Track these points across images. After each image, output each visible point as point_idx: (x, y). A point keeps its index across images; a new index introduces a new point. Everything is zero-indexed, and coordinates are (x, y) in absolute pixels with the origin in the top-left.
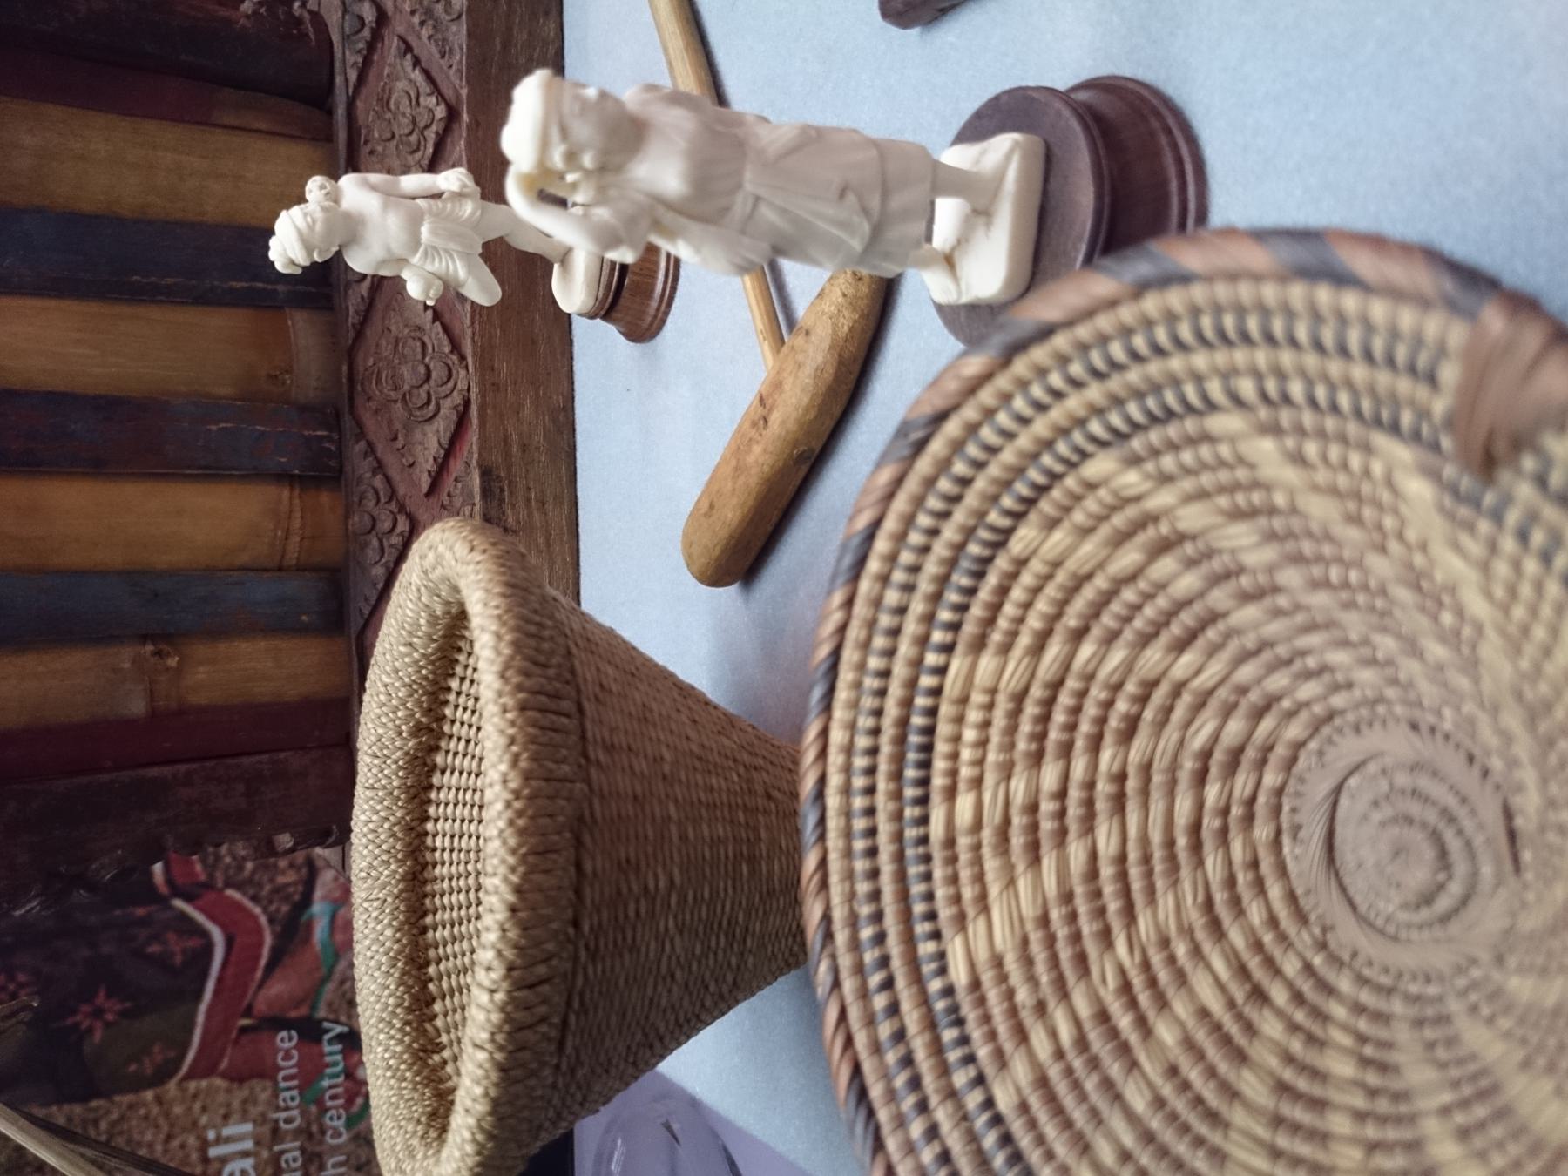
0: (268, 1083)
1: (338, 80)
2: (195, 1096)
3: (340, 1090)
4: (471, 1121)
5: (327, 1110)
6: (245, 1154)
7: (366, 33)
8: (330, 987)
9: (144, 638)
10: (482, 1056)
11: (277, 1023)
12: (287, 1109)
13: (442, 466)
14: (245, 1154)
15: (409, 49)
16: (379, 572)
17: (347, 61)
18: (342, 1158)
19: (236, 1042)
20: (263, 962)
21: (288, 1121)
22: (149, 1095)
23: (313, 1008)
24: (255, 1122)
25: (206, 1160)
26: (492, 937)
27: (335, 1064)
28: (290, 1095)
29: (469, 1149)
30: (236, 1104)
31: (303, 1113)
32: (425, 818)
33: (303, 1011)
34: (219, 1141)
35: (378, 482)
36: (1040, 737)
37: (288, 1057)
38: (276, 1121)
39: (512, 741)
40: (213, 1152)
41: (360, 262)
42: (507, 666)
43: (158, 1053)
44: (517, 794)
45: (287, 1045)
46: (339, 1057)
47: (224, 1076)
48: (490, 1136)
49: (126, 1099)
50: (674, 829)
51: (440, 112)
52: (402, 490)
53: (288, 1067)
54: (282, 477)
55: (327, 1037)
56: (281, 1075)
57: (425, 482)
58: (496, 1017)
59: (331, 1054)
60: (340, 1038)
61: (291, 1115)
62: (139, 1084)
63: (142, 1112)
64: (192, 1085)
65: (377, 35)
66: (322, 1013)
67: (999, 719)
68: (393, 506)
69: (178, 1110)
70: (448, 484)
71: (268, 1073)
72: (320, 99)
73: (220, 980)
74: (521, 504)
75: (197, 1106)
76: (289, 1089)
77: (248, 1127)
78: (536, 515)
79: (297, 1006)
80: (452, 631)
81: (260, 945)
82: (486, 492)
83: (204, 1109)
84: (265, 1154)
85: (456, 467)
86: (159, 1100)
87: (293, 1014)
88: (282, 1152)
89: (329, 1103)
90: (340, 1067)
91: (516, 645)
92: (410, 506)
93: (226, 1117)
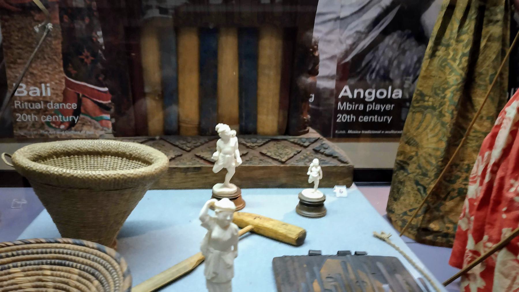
0: (62, 101)
1: (291, 137)
2: (60, 81)
3: (58, 120)
4: (32, 166)
5: (52, 116)
6: (41, 93)
7: (302, 143)
8: (89, 118)
9: (162, 92)
10: (45, 169)
11: (79, 102)
12: (54, 106)
13: (202, 158)
14: (41, 93)
15: (299, 153)
16: (177, 143)
17: (296, 139)
18: (37, 120)
19: (76, 93)
20: (98, 101)
21: (50, 106)
22: (62, 69)
23: (83, 114)
24: (50, 97)
25: (41, 83)
26: (68, 172)
27: (66, 119)
28: (57, 106)
29: (27, 165)
30: (57, 92)
31: (52, 110)
32: (112, 156)
33: (82, 111)
34: (46, 87)
35: (199, 144)
36: (84, 270)
37: (69, 106)
38: (50, 102)
39: (108, 176)
40: (43, 85)
41: (219, 142)
42: (125, 175)
43: (74, 72)
44: (96, 177)
45: (73, 106)
46: (67, 120)
47: (66, 89)
48: (29, 169)
49: (61, 63)
50: (90, 209)
51: (283, 160)
52: (196, 149)
53: (67, 106)
54: (200, 123)
55: (74, 117)
56: (64, 104)
57: (198, 154)
58: (52, 172)
59: (69, 118)
60: (73, 121)
61: (51, 106)
62: (65, 66)
63: (57, 67)
64: (64, 81)
65: (301, 146)
66: (82, 116)
67: (89, 262)
68: (193, 147)
69: (57, 76)
70: (198, 159)
71: (65, 101)
72: (287, 132)
73: (93, 89)
74: (193, 176)
75: (57, 81)
76: (60, 106)
77: (49, 94)
78: (190, 180)
79: (85, 109)
80: (148, 162)
81: (104, 100)
82: (195, 168)
83: (56, 83)
84: (41, 99)
85: (202, 161)
86: (61, 72)
87: (82, 108)
88: (41, 104)
89: (54, 117)
90: (65, 121)
91: (129, 178)
92: (193, 151)
93: (53, 89)
